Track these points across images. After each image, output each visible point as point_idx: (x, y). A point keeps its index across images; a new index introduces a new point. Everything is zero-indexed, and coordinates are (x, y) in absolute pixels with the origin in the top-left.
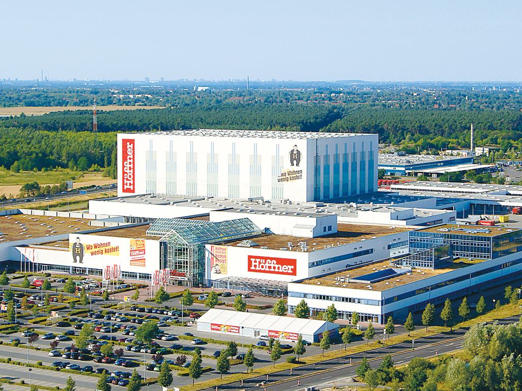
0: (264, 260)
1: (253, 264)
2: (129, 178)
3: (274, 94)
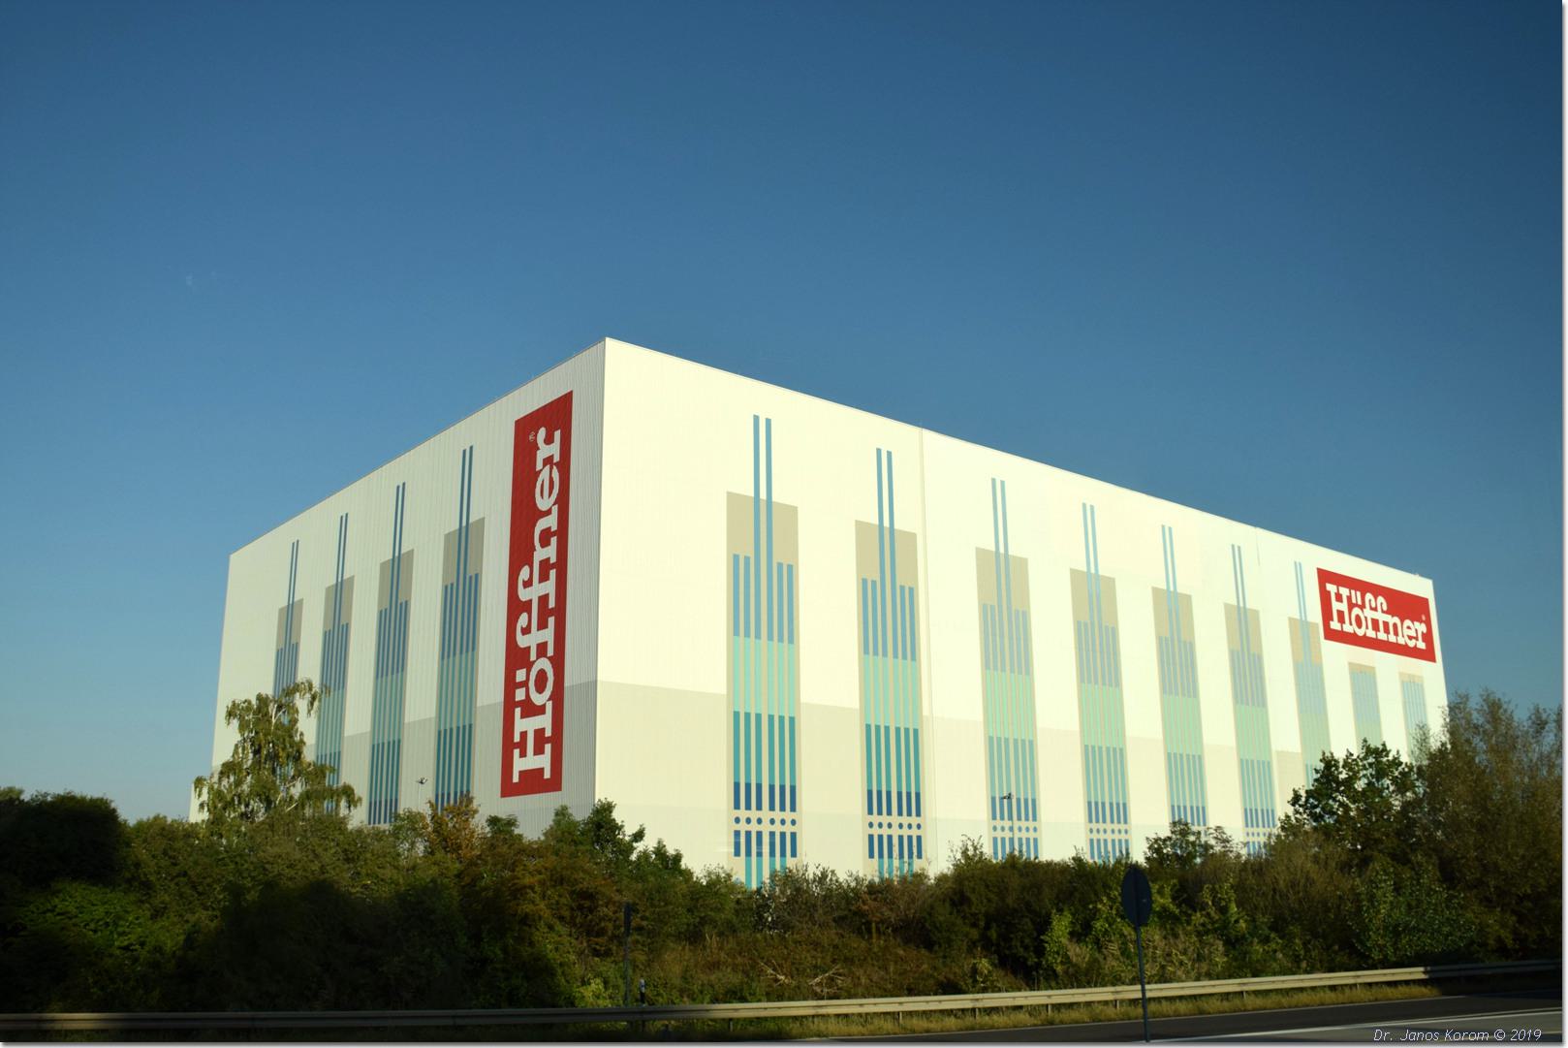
1: (1336, 606)
2: (538, 699)
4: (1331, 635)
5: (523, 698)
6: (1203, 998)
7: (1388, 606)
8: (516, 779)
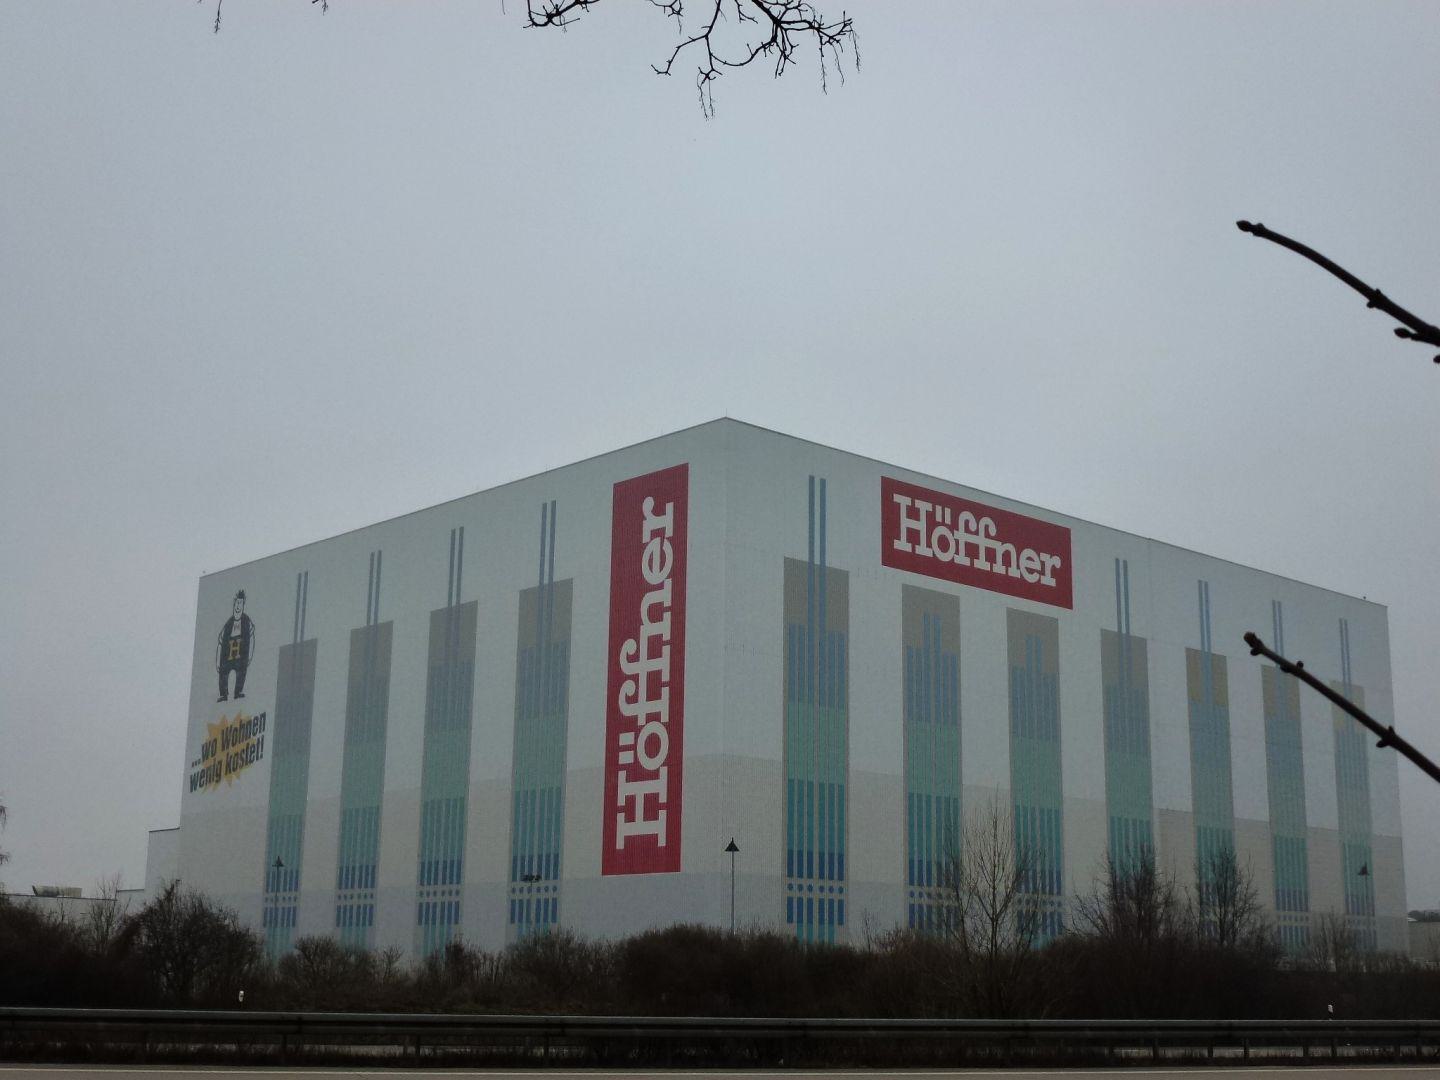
1: (906, 523)
2: (649, 764)
4: (892, 558)
5: (632, 761)
7: (997, 526)
8: (620, 845)
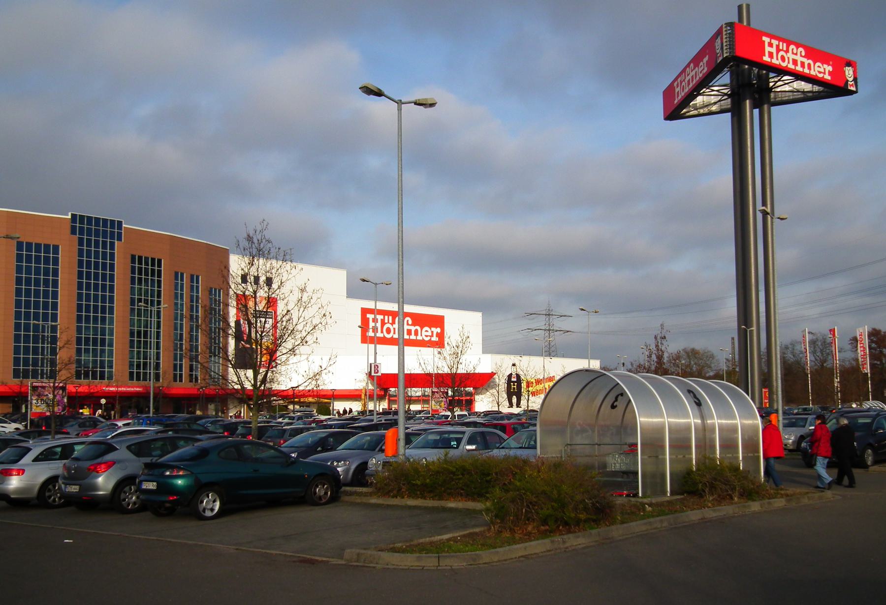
0: (390, 318)
1: (372, 324)
3: (206, 342)
6: (420, 446)
